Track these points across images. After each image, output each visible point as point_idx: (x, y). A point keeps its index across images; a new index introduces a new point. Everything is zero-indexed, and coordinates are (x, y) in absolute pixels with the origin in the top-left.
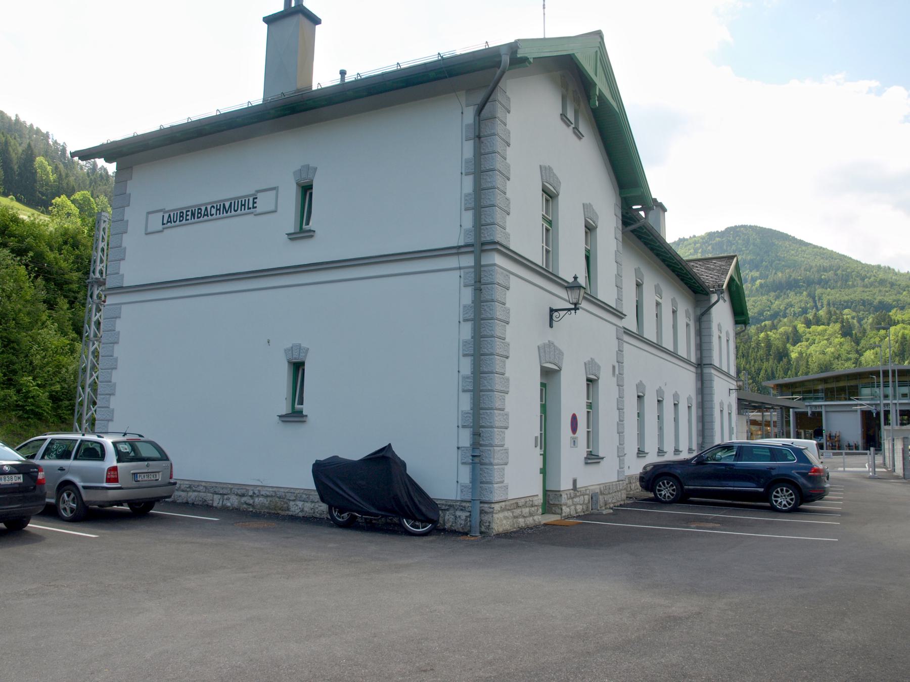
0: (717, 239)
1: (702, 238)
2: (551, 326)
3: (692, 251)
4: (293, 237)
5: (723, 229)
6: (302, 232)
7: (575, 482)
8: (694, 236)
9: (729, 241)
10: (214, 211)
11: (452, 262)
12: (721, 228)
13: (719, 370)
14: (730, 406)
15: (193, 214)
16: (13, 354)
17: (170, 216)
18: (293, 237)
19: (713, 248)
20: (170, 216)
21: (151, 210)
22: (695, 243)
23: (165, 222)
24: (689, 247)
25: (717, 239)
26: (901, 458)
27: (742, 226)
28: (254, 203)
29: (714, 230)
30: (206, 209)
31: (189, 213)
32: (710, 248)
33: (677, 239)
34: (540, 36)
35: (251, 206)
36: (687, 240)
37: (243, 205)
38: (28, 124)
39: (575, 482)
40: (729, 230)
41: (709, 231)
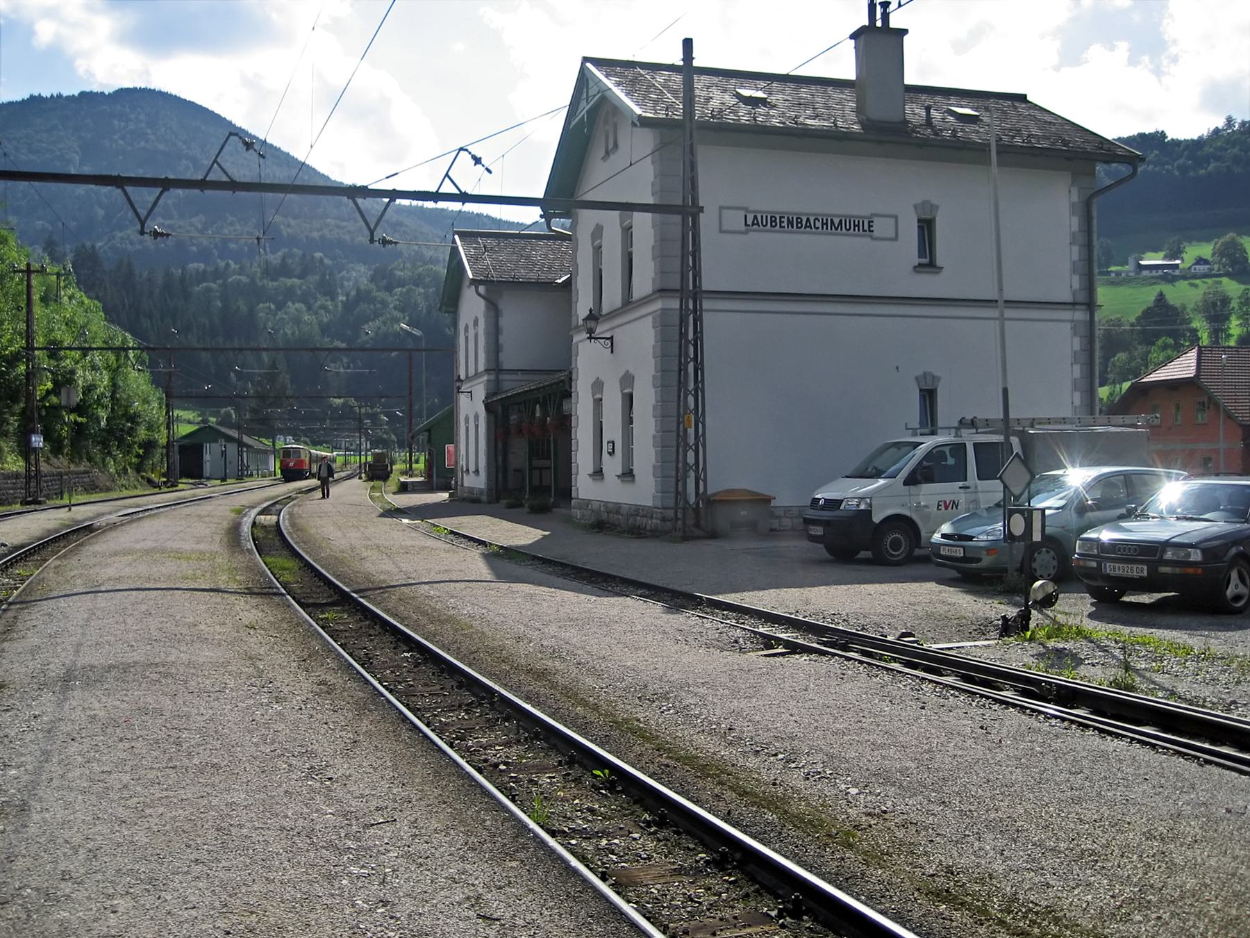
4: (919, 268)
6: (928, 263)
7: (688, 44)
10: (819, 224)
11: (1066, 315)
13: (161, 193)
14: (477, 417)
15: (790, 222)
17: (755, 217)
18: (919, 268)
20: (755, 217)
21: (725, 205)
23: (749, 222)
28: (870, 226)
30: (808, 220)
31: (785, 220)
34: (301, 159)
35: (866, 227)
37: (860, 226)
39: (688, 44)
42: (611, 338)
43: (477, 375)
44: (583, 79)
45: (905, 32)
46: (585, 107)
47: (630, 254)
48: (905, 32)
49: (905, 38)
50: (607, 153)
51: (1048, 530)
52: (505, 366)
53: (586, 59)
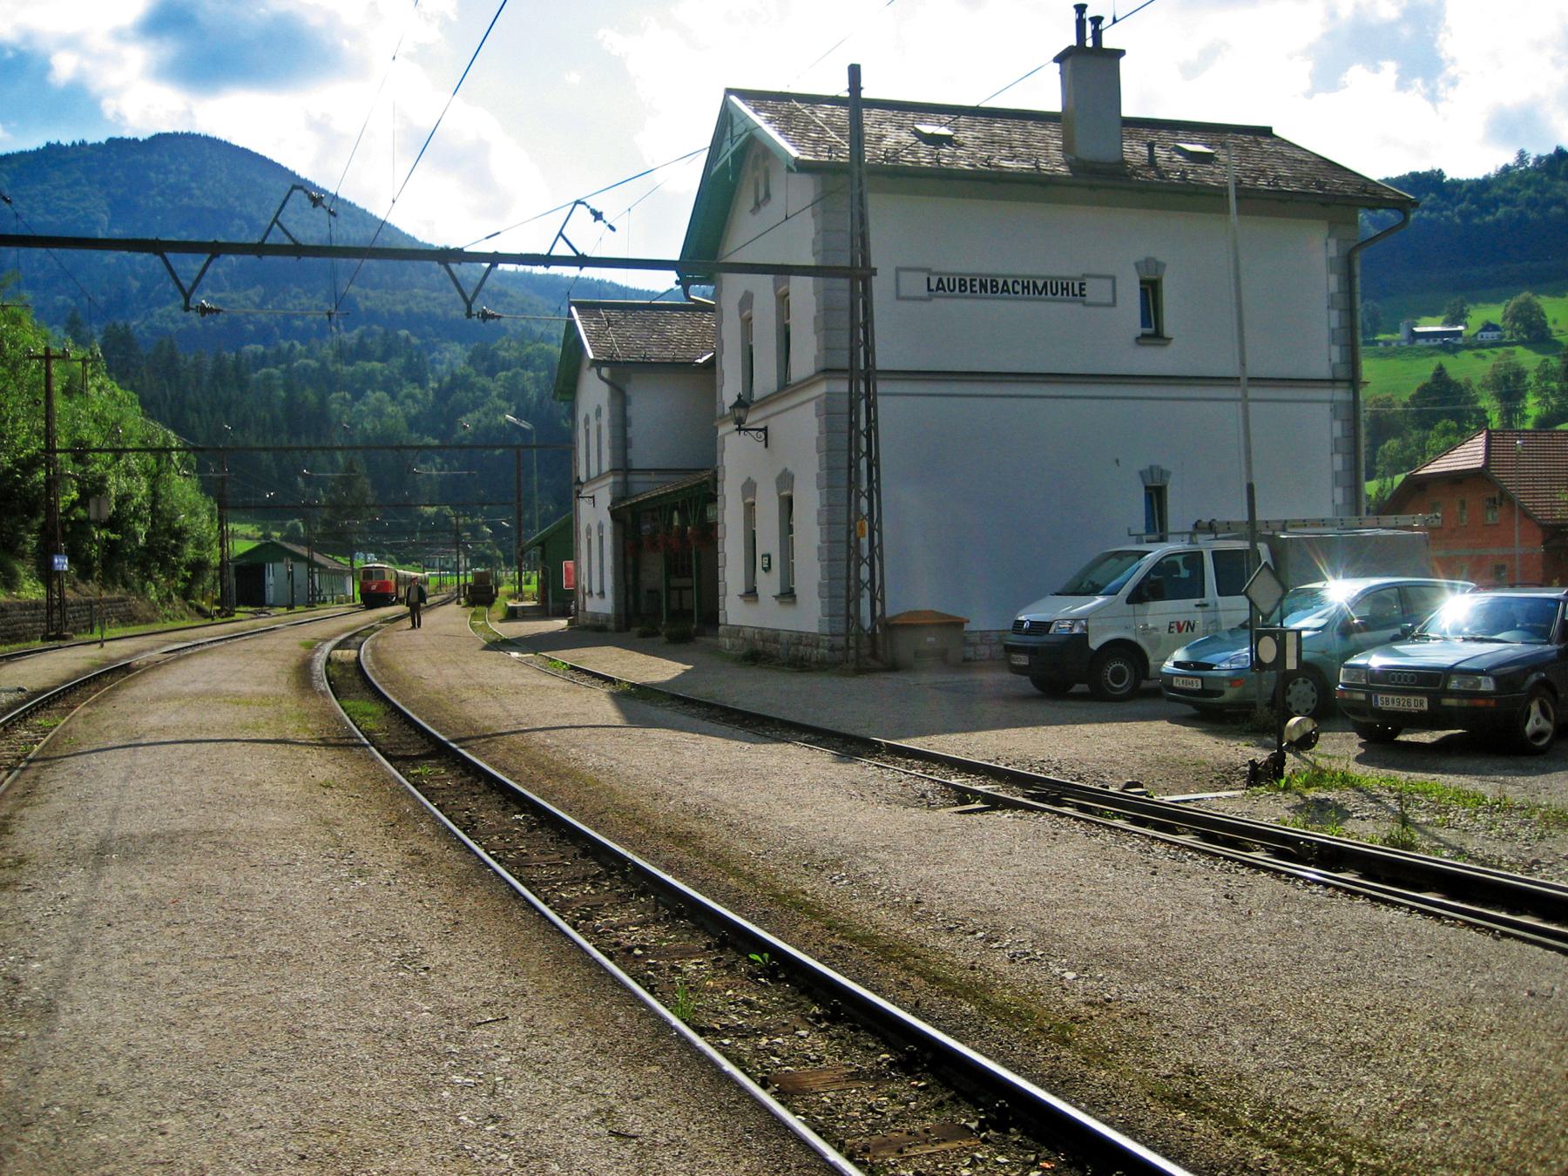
42: (765, 430)
43: (601, 476)
44: (727, 117)
45: (1121, 53)
46: (729, 149)
47: (787, 327)
48: (1121, 53)
49: (1123, 61)
50: (758, 205)
51: (1305, 656)
52: (636, 465)
53: (729, 91)
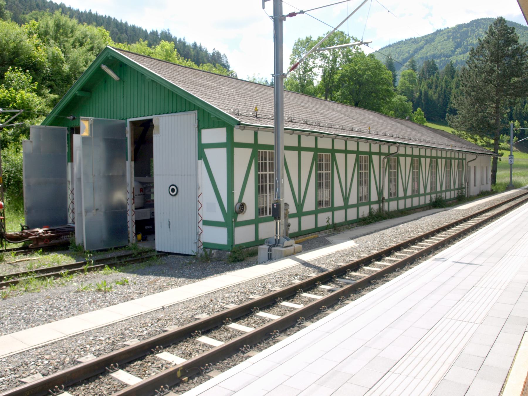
0: (464, 29)
1: (454, 28)
2: (264, 8)
3: (446, 38)
5: (469, 22)
8: (448, 28)
9: (473, 30)
11: (324, 191)
12: (467, 21)
16: (63, 52)
19: (460, 35)
22: (448, 32)
24: (444, 35)
25: (464, 29)
26: (513, 205)
27: (482, 19)
29: (462, 22)
32: (458, 35)
33: (435, 31)
36: (443, 30)
38: (104, 16)
40: (472, 22)
41: (459, 24)
